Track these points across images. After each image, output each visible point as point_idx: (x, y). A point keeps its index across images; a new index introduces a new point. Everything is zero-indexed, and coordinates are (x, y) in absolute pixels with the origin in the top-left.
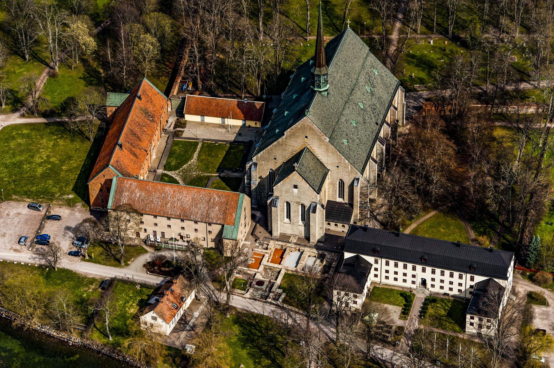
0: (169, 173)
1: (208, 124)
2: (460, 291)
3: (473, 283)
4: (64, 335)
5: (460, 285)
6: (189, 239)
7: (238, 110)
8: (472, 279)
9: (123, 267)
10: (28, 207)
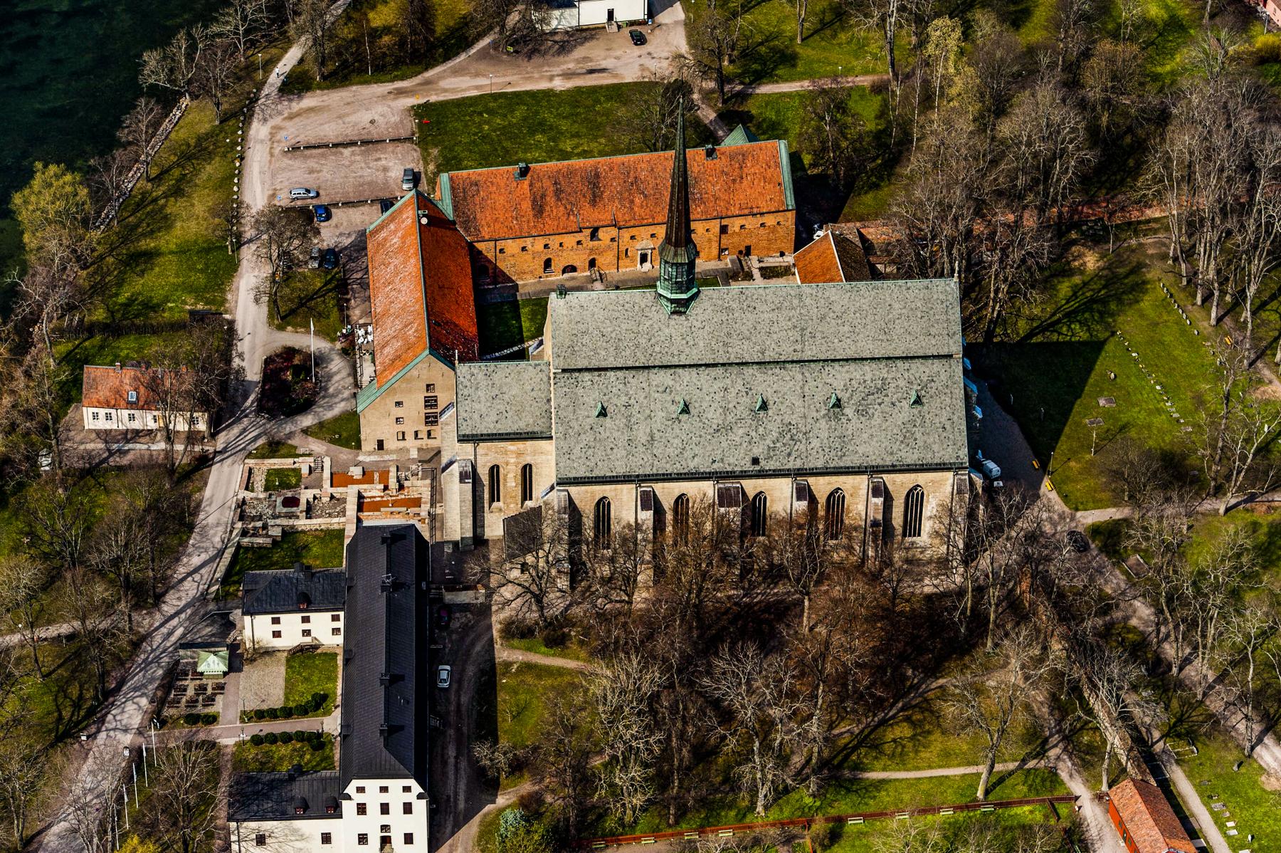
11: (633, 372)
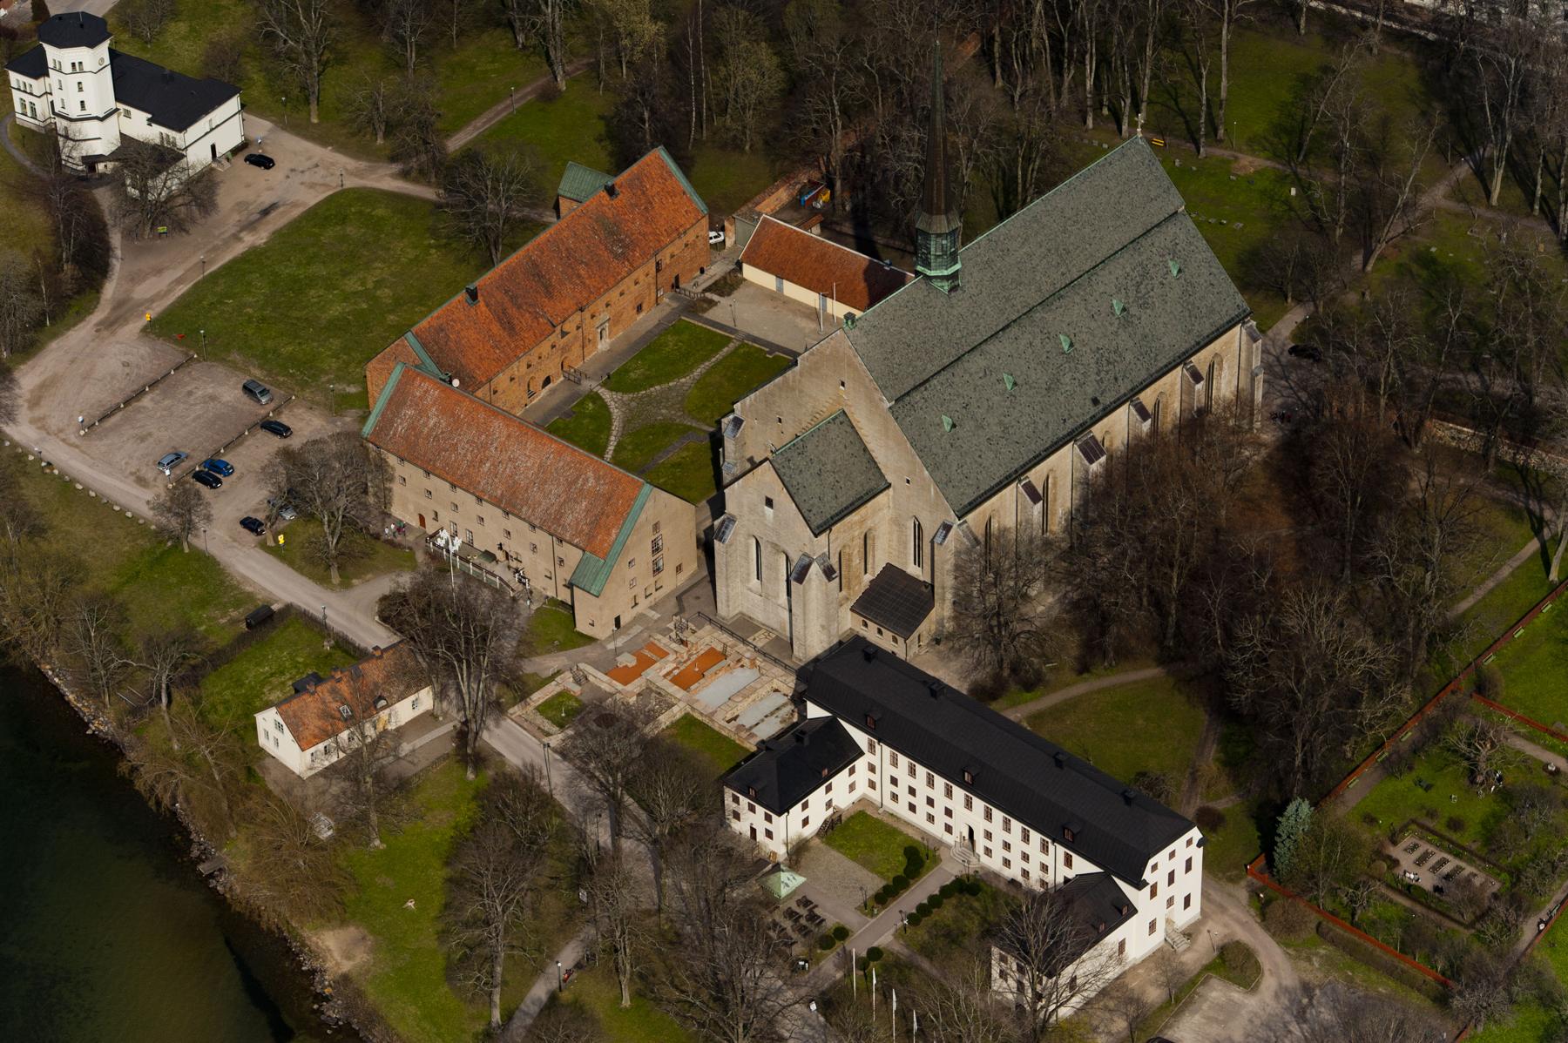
0: (606, 395)
1: (788, 302)
2: (1043, 883)
3: (1071, 874)
4: (84, 707)
5: (1044, 868)
6: (520, 566)
7: (863, 284)
8: (1068, 862)
9: (332, 588)
10: (245, 388)
11: (951, 370)
